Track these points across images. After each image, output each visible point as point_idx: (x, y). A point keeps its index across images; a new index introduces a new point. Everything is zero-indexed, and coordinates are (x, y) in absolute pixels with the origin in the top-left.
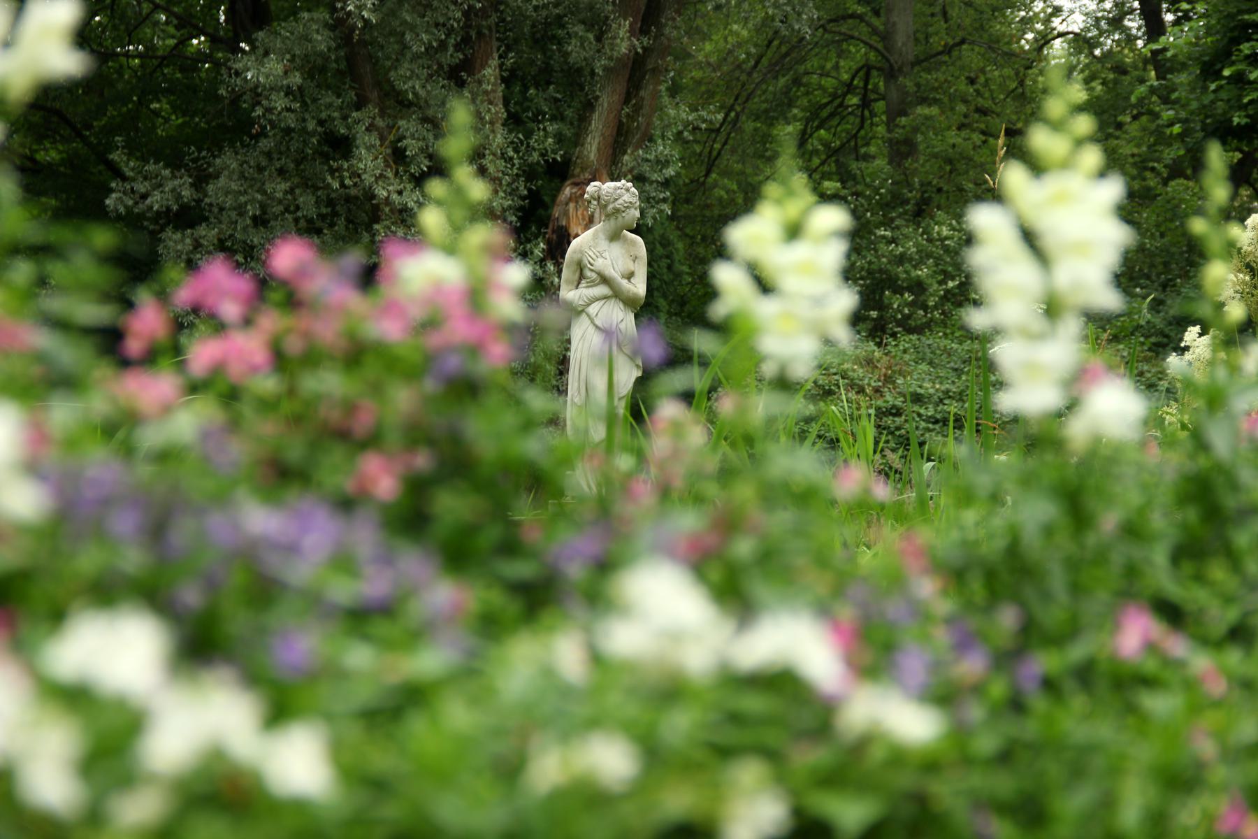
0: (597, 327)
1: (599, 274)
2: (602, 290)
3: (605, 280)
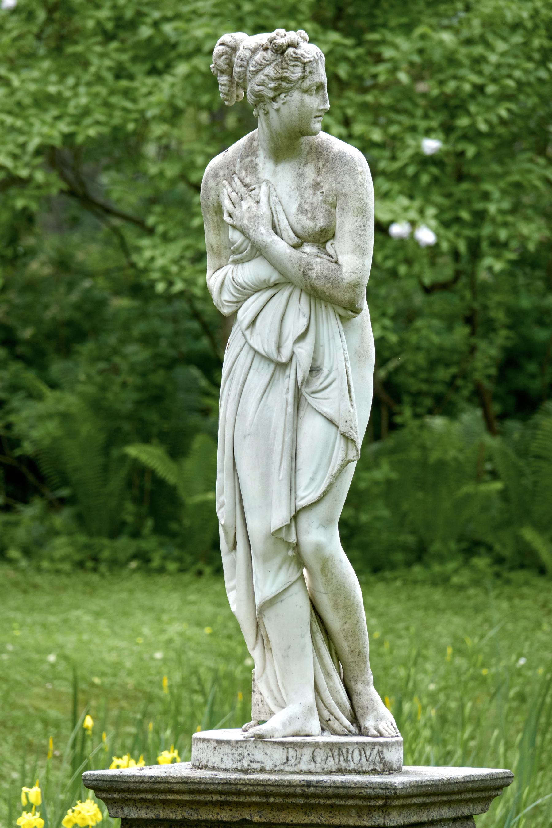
0: (256, 352)
3: (258, 251)
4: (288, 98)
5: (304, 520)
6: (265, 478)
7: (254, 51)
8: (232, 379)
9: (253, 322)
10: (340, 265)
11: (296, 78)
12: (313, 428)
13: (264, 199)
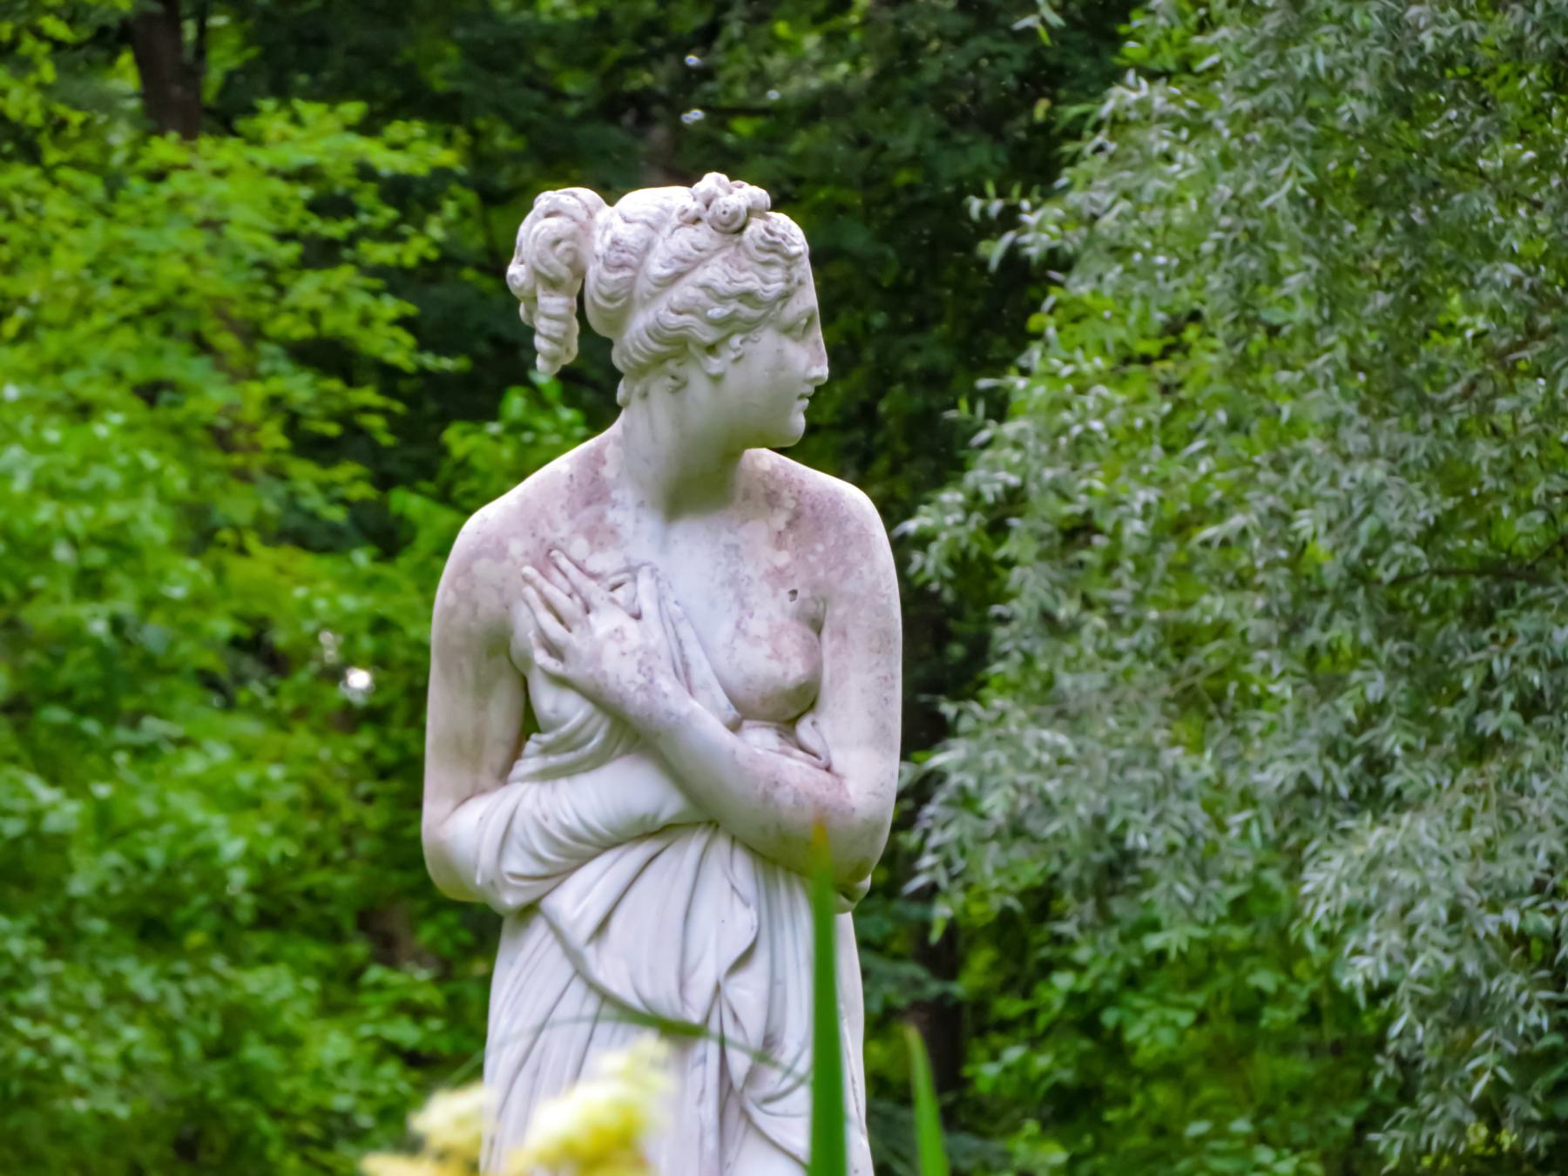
0: (605, 997)
1: (597, 698)
2: (623, 789)
3: (631, 732)
4: (749, 346)
8: (536, 1072)
10: (838, 776)
11: (771, 295)
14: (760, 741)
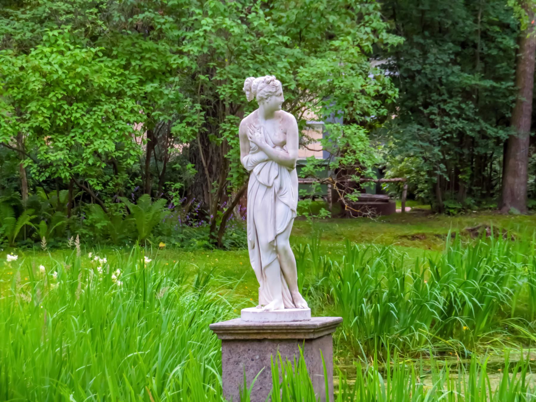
0: (260, 183)
3: (260, 149)
5: (279, 238)
6: (266, 224)
7: (258, 83)
9: (259, 173)
12: (281, 208)
13: (262, 132)
14: (278, 149)
